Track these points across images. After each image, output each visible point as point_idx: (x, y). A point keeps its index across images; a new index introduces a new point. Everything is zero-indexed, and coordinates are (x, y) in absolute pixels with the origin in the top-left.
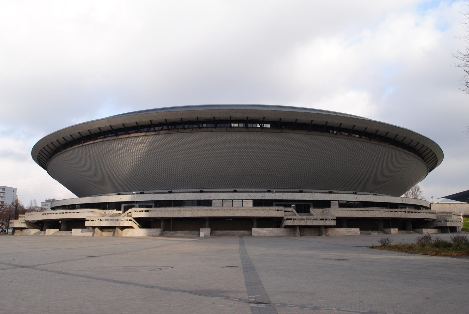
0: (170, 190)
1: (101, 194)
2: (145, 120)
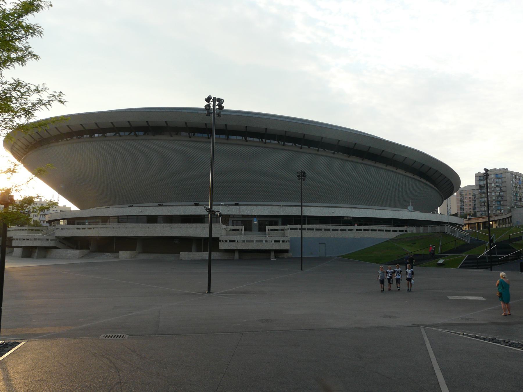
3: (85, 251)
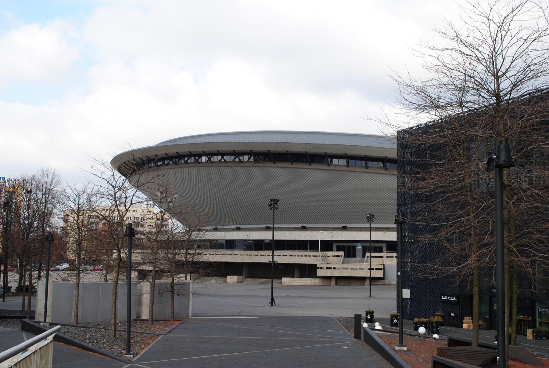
3: (241, 277)
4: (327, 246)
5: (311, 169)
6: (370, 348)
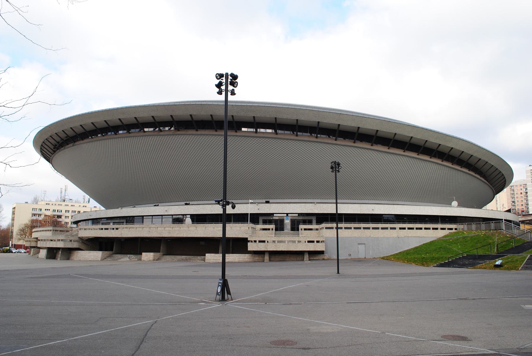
0: (188, 202)
1: (134, 204)
2: (184, 114)
3: (158, 254)
4: (255, 218)
5: (237, 136)
6: (133, 256)
